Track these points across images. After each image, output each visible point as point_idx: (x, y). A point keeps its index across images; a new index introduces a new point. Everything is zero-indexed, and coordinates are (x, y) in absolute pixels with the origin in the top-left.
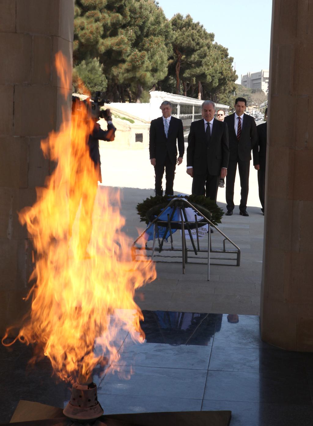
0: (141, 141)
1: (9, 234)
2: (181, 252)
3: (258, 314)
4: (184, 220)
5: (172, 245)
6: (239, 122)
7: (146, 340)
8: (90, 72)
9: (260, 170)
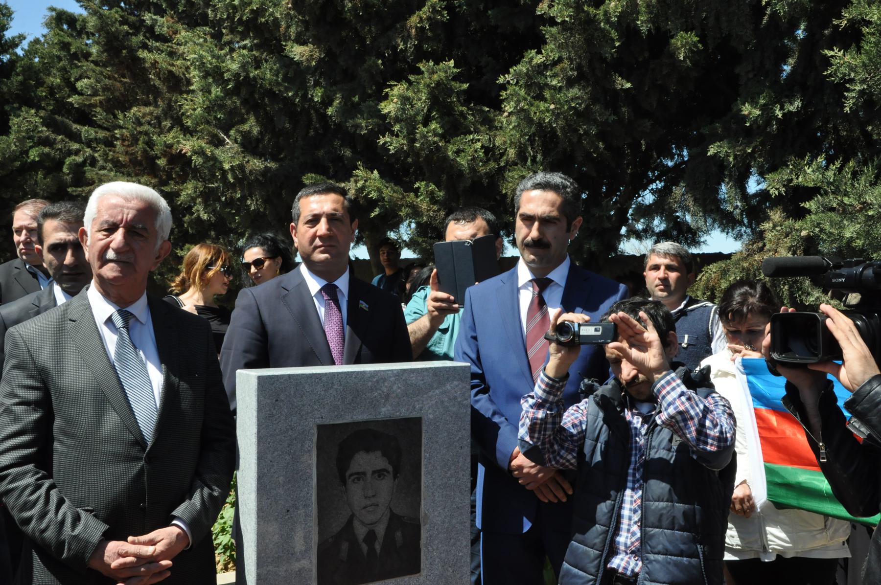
4: (31, 466)
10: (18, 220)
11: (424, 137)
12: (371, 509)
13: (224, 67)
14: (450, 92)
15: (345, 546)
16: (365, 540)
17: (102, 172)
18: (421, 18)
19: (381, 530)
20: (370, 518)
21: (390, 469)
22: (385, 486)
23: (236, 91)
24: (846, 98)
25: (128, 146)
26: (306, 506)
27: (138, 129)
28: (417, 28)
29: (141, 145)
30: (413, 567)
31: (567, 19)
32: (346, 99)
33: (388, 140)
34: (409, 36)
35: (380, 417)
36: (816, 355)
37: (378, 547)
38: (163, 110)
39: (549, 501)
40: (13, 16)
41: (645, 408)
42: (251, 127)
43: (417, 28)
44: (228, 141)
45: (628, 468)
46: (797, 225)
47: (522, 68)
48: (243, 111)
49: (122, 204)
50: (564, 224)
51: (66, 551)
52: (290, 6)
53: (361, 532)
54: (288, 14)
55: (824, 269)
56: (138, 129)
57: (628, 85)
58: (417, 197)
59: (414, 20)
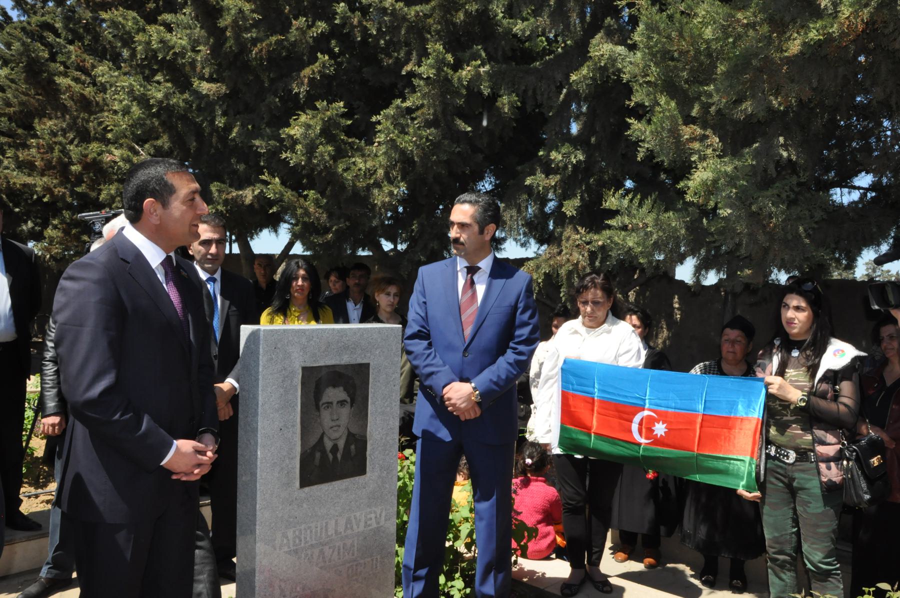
11: (322, 156)
12: (335, 429)
13: (150, 95)
14: (337, 125)
15: (318, 455)
16: (331, 451)
17: (6, 171)
18: (313, 71)
19: (341, 444)
20: (335, 435)
21: (349, 400)
22: (345, 411)
23: (157, 115)
25: (44, 153)
26: (293, 426)
27: (53, 139)
28: (309, 78)
29: (56, 153)
30: (362, 471)
31: (432, 76)
32: (243, 126)
33: (289, 155)
34: (302, 84)
35: (343, 363)
37: (339, 456)
38: (68, 124)
42: (163, 143)
43: (309, 78)
44: (142, 152)
46: (596, 237)
47: (390, 111)
48: (160, 130)
50: (476, 228)
52: (208, 52)
53: (329, 445)
54: (207, 58)
56: (53, 139)
57: (469, 129)
58: (306, 200)
59: (307, 72)
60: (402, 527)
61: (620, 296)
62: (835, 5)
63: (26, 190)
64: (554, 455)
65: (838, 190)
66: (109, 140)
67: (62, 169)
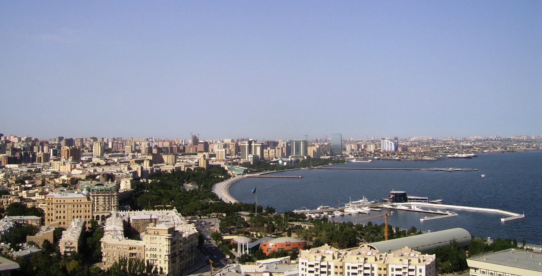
0: (411, 260)
1: (236, 161)
2: (43, 196)
3: (288, 247)
4: (50, 149)
5: (307, 138)
6: (55, 157)
7: (219, 267)
8: (105, 224)
9: (56, 246)
10: (242, 266)
24: (488, 239)
36: (250, 254)
39: (232, 250)
40: (46, 239)
41: (300, 154)
45: (159, 205)
49: (28, 203)
51: (363, 162)
55: (234, 257)
60: (169, 250)
61: (190, 185)
62: (1, 181)
63: (107, 153)
64: (224, 240)
65: (209, 163)
66: (473, 142)
67: (497, 225)
